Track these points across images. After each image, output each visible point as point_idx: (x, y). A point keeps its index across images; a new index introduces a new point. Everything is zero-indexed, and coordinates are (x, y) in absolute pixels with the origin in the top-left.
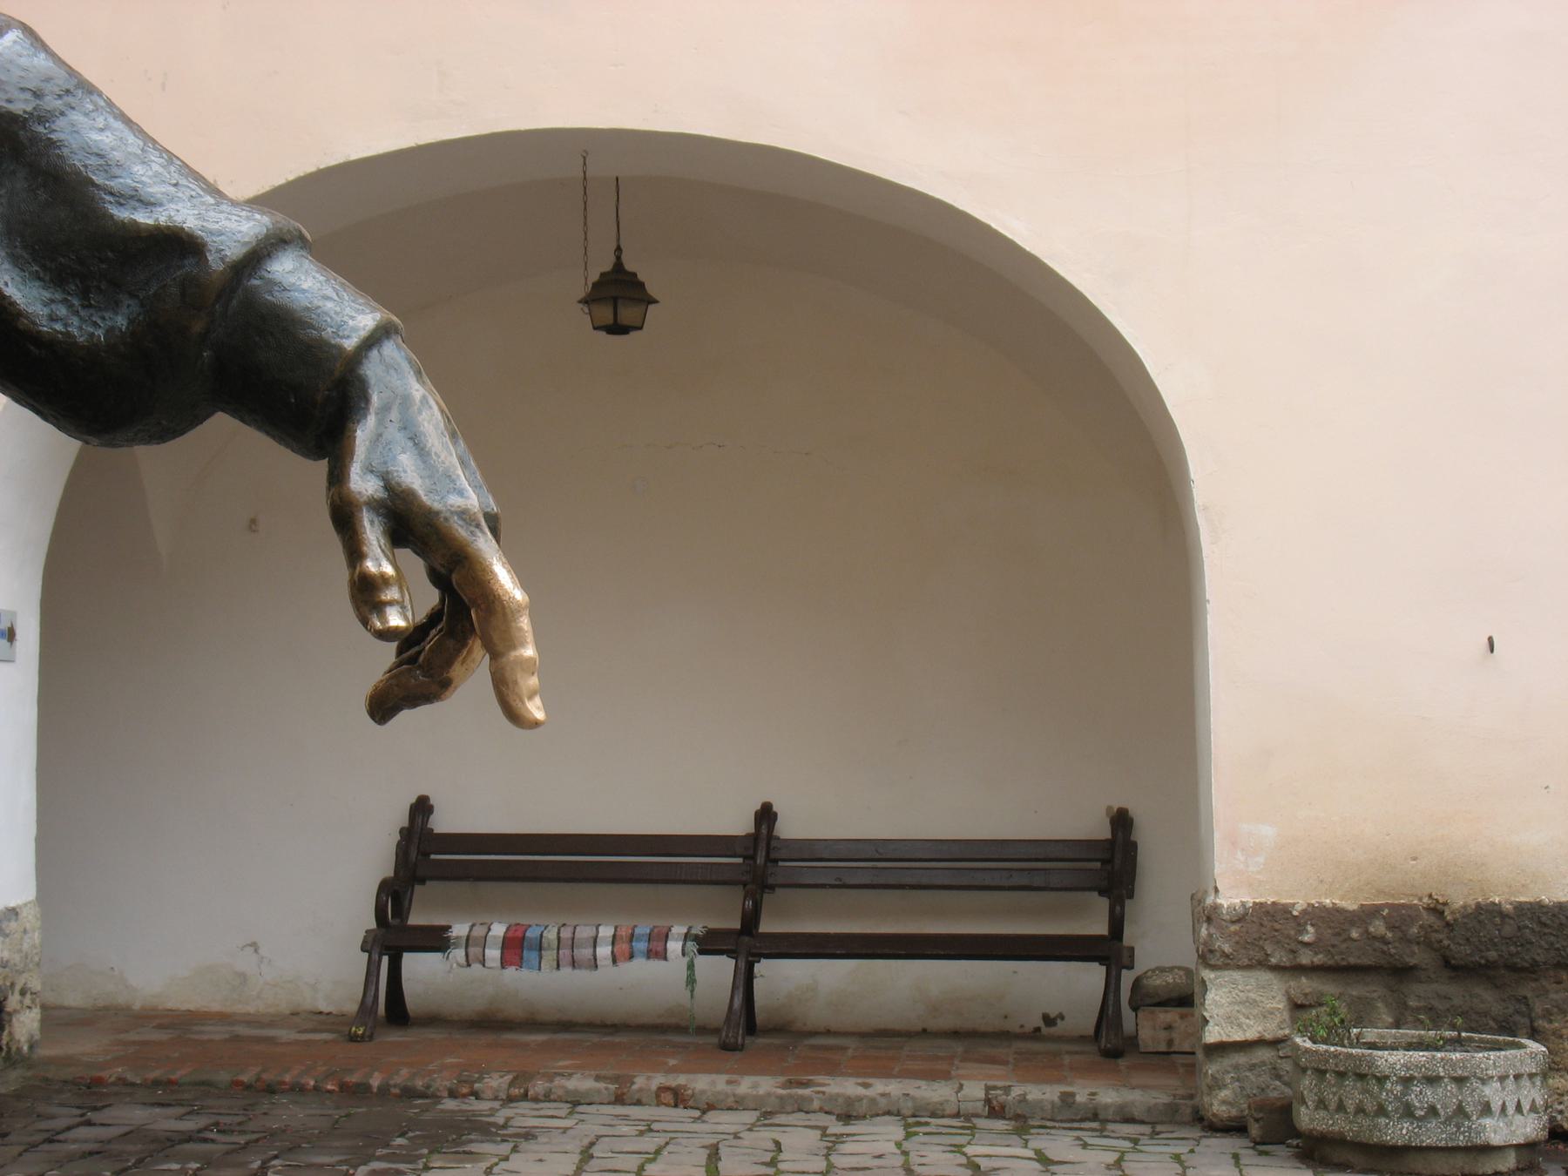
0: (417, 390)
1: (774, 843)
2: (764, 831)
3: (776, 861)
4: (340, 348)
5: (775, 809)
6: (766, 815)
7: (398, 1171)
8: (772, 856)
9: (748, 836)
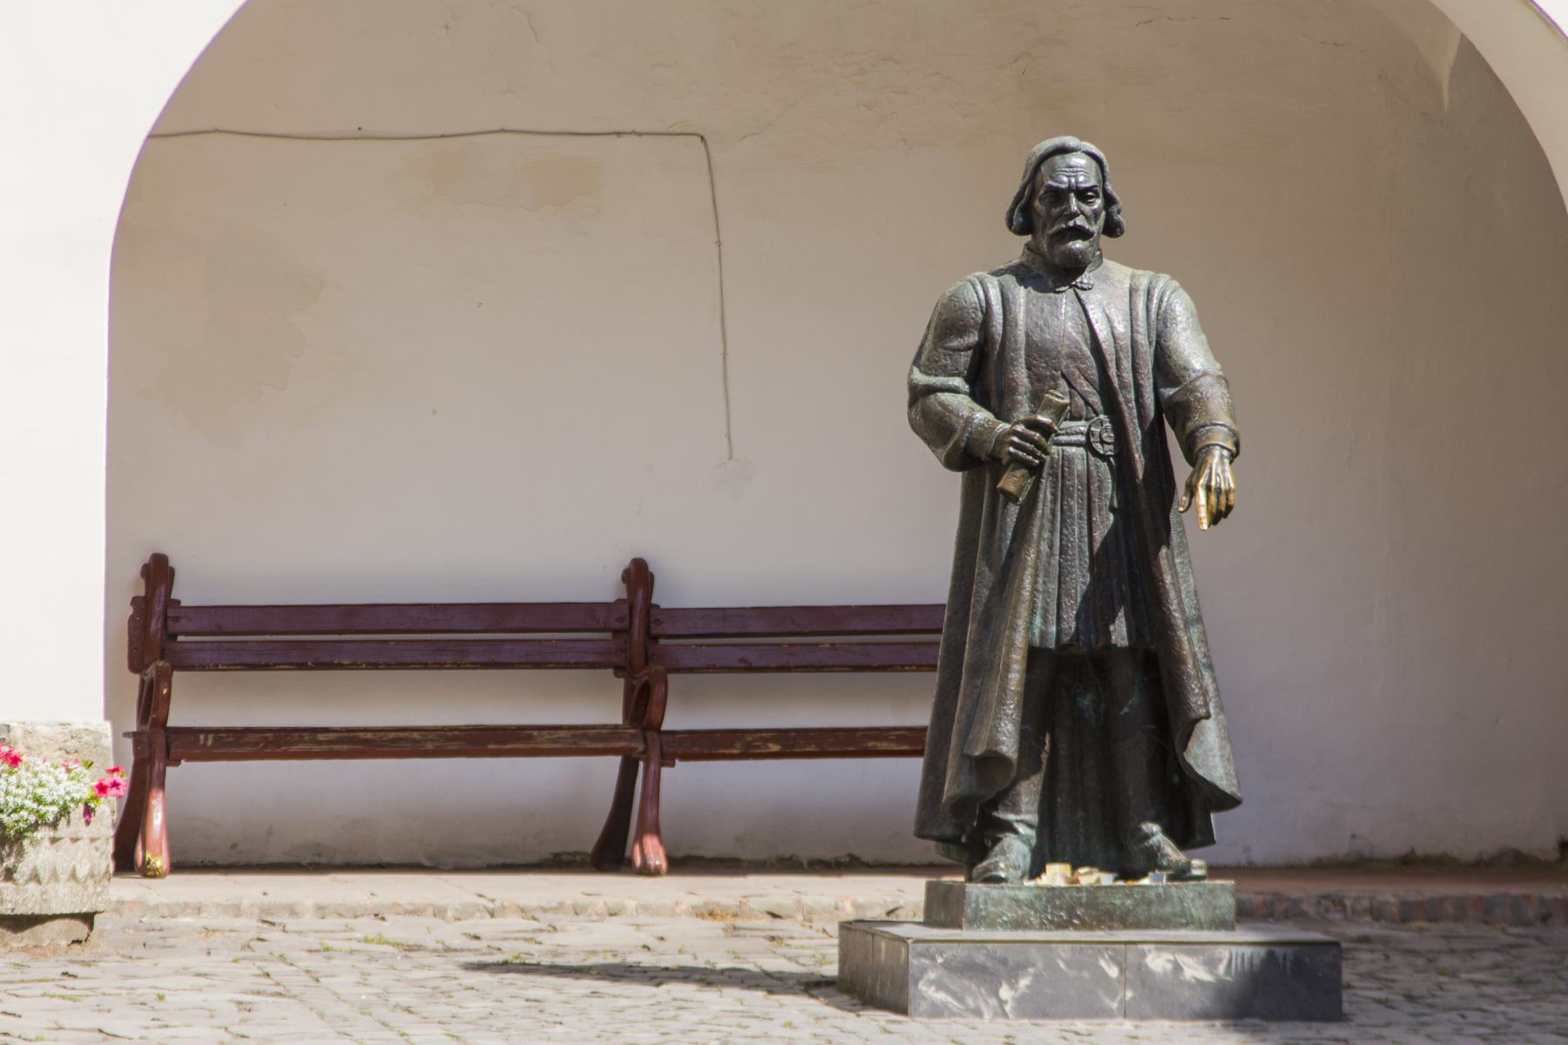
5: (651, 569)
6: (639, 575)
8: (655, 630)
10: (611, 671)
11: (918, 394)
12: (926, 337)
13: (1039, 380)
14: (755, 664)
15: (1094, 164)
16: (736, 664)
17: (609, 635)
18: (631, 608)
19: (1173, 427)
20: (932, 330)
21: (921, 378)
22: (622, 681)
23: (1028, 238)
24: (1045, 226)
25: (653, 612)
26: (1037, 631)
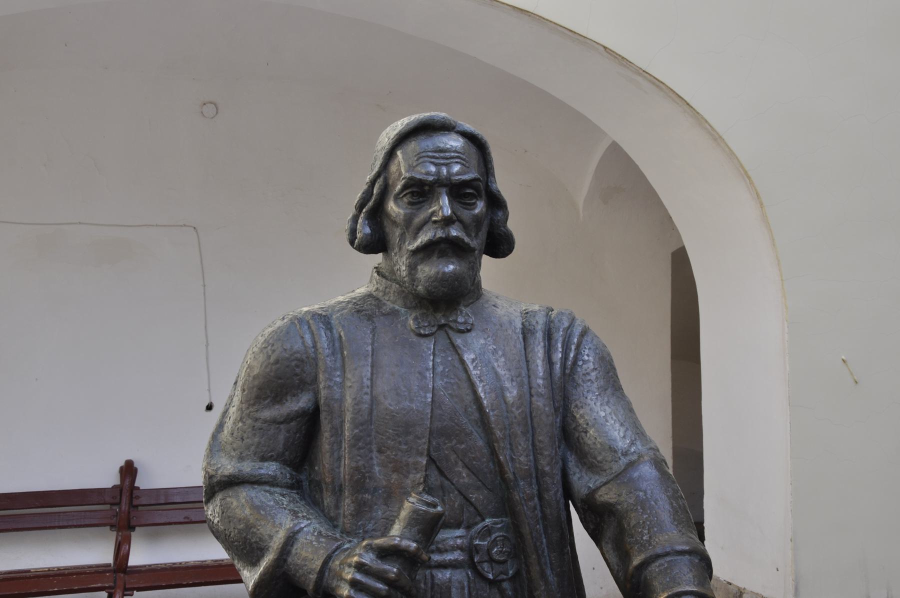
0: (482, 395)
1: (135, 493)
2: (127, 482)
3: (137, 506)
4: (371, 235)
5: (136, 465)
6: (129, 470)
7: (310, 306)
8: (135, 502)
9: (115, 487)
10: (108, 527)
12: (231, 398)
13: (395, 470)
14: (193, 519)
15: (473, 150)
16: (182, 520)
17: (108, 507)
18: (121, 491)
19: (596, 535)
20: (238, 392)
22: (115, 533)
23: (379, 258)
24: (402, 237)
25: (134, 492)
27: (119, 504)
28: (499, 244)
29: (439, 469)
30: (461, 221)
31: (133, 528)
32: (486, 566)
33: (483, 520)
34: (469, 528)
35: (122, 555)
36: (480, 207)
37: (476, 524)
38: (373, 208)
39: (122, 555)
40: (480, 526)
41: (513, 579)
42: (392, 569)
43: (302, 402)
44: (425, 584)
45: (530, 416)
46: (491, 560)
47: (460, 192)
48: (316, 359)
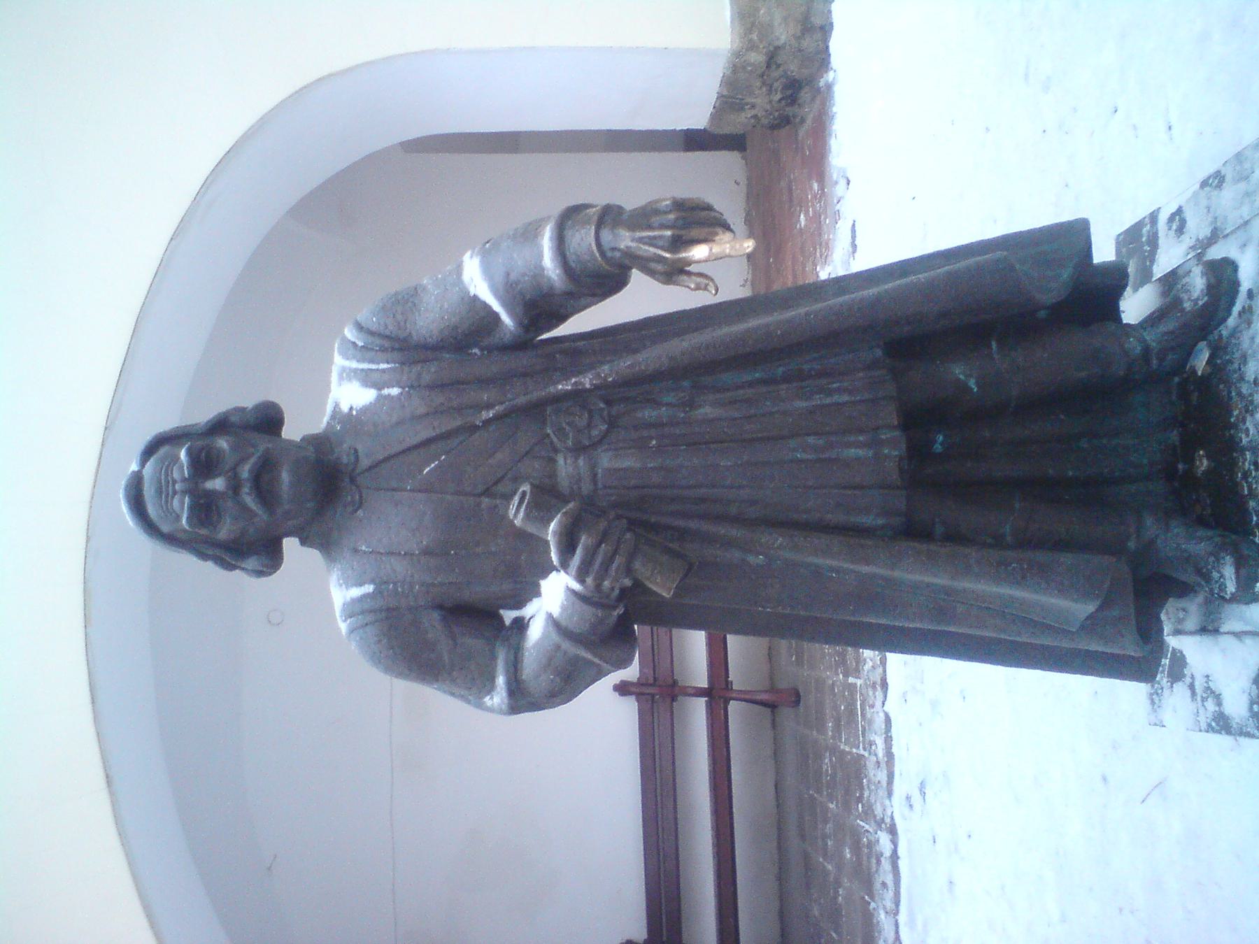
2: (633, 689)
3: (655, 679)
8: (651, 681)
11: (522, 699)
21: (498, 698)
26: (880, 522)
27: (653, 696)
28: (268, 420)
29: (496, 483)
30: (237, 465)
31: (675, 683)
32: (595, 432)
33: (548, 435)
34: (556, 451)
35: (700, 693)
36: (223, 443)
37: (552, 443)
38: (231, 553)
39: (700, 693)
40: (555, 440)
41: (609, 403)
42: (584, 540)
43: (432, 622)
44: (611, 495)
45: (431, 387)
46: (589, 426)
47: (204, 464)
48: (388, 609)
